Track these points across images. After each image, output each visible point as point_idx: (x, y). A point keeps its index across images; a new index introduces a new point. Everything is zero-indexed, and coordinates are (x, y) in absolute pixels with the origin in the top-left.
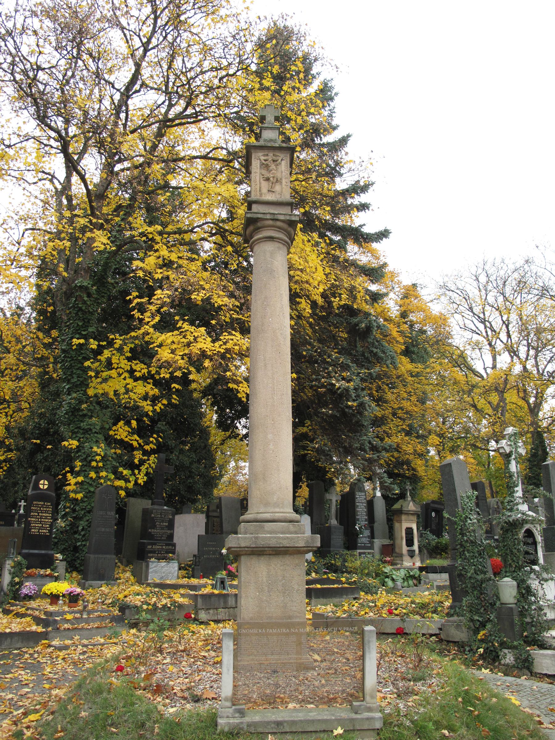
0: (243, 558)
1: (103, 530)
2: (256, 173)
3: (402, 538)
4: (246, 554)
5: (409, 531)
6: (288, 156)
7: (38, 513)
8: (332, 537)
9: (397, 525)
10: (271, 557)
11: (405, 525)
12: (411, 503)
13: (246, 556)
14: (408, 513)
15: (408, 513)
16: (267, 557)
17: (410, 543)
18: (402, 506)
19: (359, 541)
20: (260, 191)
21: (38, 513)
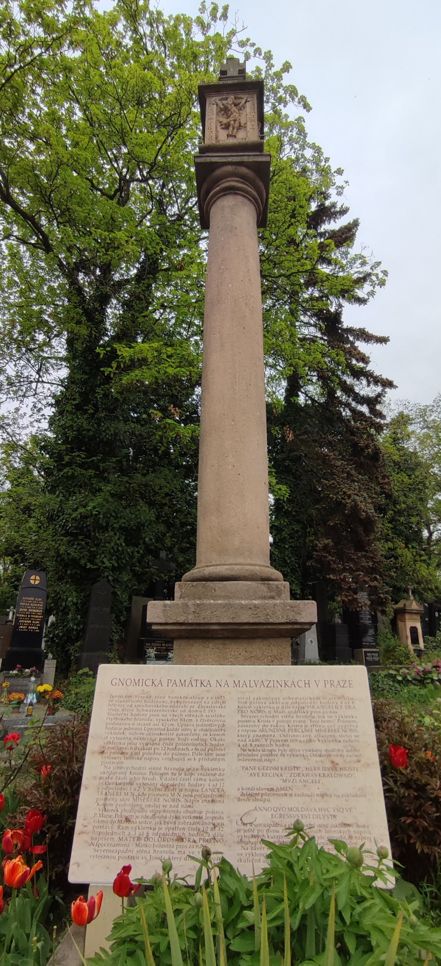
0: (176, 644)
1: (97, 626)
2: (211, 119)
3: (407, 637)
4: (180, 637)
5: (414, 630)
6: (255, 96)
7: (28, 609)
8: (337, 635)
9: (400, 624)
10: (227, 642)
11: (409, 624)
12: (414, 602)
13: (183, 642)
14: (411, 613)
15: (411, 613)
16: (219, 643)
17: (415, 640)
18: (405, 605)
19: (364, 640)
20: (216, 138)
21: (28, 609)
